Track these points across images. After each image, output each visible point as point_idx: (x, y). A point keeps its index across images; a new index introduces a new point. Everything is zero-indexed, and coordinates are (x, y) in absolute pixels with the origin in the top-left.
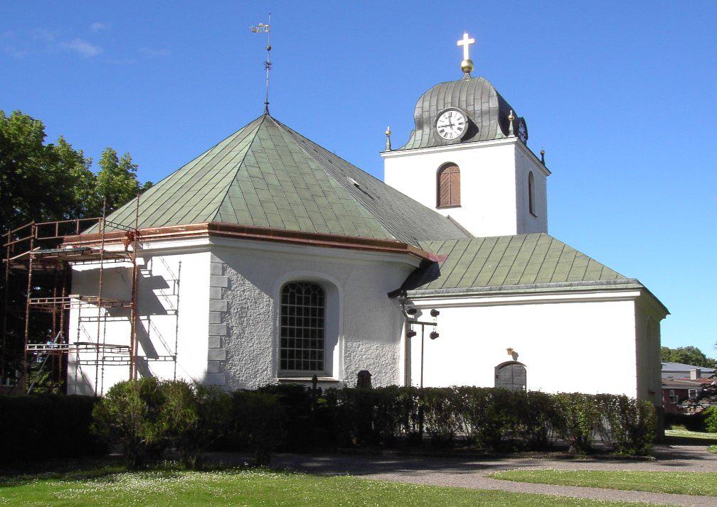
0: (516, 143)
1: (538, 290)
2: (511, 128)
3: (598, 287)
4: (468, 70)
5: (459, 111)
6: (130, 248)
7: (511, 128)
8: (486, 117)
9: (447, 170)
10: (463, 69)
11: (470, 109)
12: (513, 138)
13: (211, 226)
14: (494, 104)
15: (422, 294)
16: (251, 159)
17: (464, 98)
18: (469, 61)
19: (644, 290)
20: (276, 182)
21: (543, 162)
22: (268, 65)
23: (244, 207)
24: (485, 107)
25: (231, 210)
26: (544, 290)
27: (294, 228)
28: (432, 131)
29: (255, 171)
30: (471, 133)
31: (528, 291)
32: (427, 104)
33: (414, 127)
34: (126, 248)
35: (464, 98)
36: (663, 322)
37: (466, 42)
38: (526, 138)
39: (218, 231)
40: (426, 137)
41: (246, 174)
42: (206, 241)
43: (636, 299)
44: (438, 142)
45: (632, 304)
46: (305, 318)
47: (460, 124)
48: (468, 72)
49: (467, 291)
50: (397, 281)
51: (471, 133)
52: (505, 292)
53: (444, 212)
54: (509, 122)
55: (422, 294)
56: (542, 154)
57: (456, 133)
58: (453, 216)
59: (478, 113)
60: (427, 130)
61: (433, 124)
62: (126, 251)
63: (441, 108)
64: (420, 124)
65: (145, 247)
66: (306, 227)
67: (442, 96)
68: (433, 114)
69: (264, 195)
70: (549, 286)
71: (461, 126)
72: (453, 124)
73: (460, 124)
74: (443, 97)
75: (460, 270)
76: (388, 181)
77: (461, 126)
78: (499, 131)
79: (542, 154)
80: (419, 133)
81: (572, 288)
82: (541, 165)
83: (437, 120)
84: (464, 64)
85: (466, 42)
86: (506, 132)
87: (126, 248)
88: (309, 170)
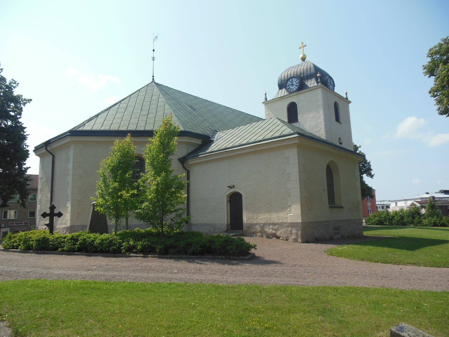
2: (319, 80)
7: (319, 80)
21: (347, 99)
22: (153, 59)
33: (277, 88)
38: (334, 86)
47: (296, 83)
56: (346, 94)
71: (297, 84)
73: (296, 83)
77: (297, 84)
79: (346, 94)
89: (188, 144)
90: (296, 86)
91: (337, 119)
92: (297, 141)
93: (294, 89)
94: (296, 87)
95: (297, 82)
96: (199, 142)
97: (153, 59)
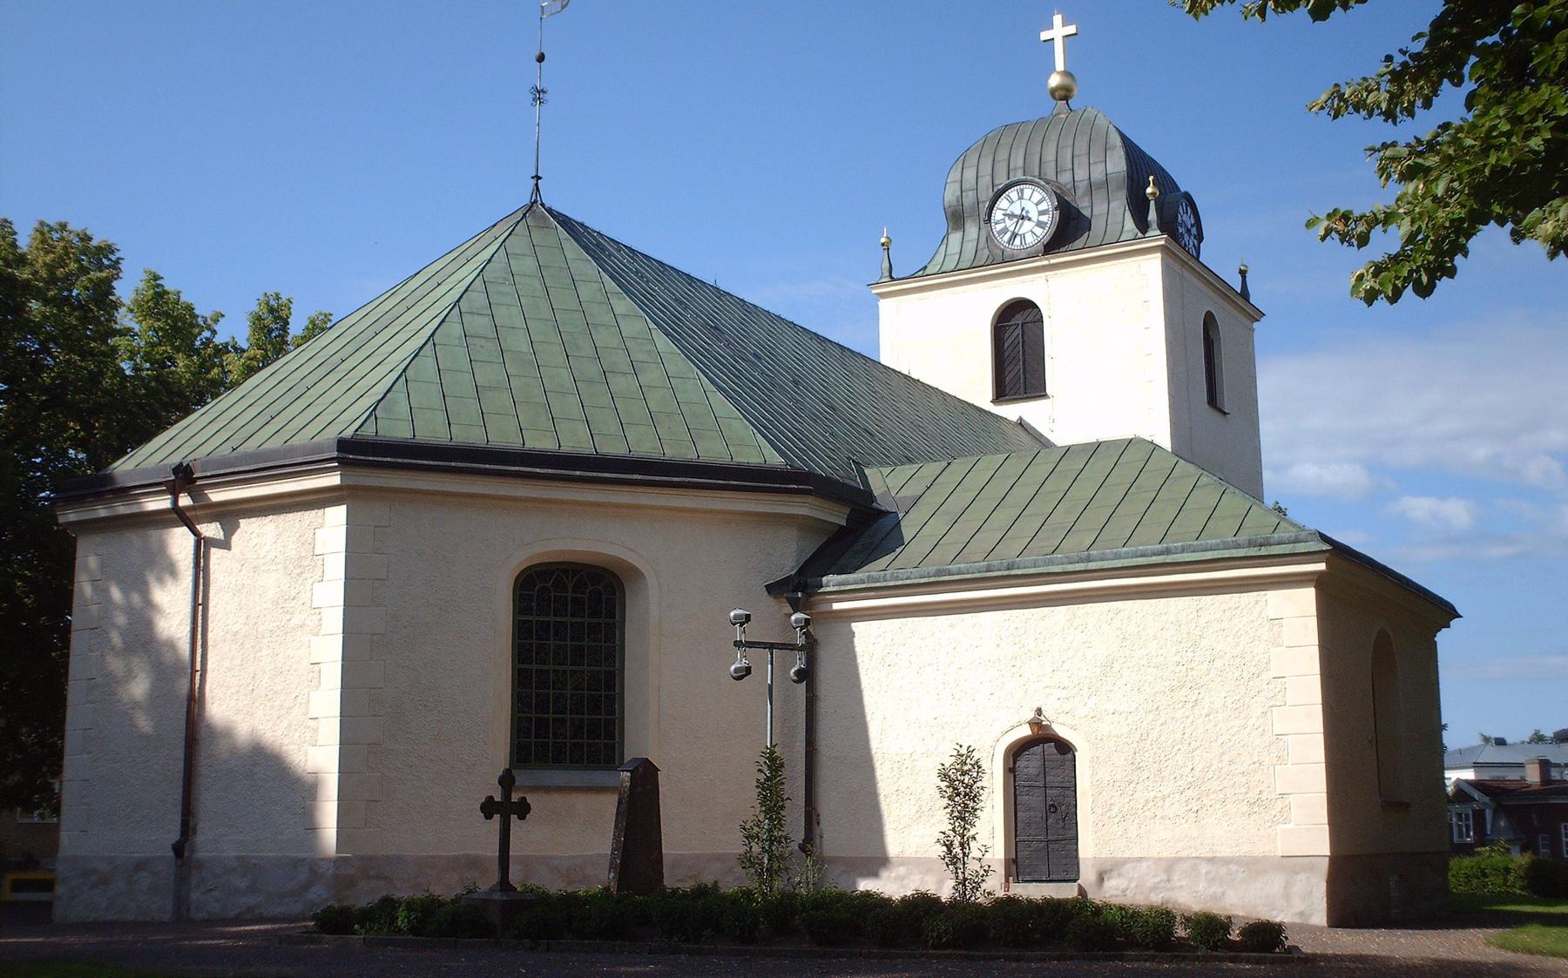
0: (1164, 249)
1: (1092, 566)
2: (1152, 216)
3: (1226, 554)
4: (1063, 93)
5: (1038, 185)
6: (185, 501)
7: (1152, 216)
8: (1099, 196)
9: (1018, 319)
10: (1053, 92)
11: (1065, 178)
12: (1156, 238)
13: (343, 445)
14: (1117, 164)
15: (840, 584)
16: (477, 299)
17: (1050, 155)
18: (1066, 73)
19: (1339, 553)
20: (525, 347)
21: (1245, 294)
22: (539, 94)
23: (436, 401)
24: (1098, 174)
25: (405, 408)
26: (1106, 564)
27: (546, 444)
28: (983, 233)
29: (480, 324)
30: (1068, 231)
31: (1070, 568)
32: (970, 175)
33: (943, 224)
34: (175, 502)
35: (1050, 155)
36: (1443, 638)
37: (1058, 31)
38: (1200, 237)
39: (356, 453)
40: (970, 248)
41: (457, 330)
42: (334, 479)
43: (1318, 581)
44: (996, 259)
45: (1308, 595)
46: (570, 661)
47: (1041, 213)
48: (1066, 98)
49: (939, 573)
50: (786, 556)
51: (1068, 231)
52: (1019, 572)
53: (1011, 411)
54: (1162, 206)
55: (840, 584)
56: (1243, 273)
57: (1034, 233)
58: (1028, 419)
59: (1082, 187)
60: (972, 230)
61: (983, 216)
62: (175, 508)
63: (1002, 181)
64: (957, 218)
65: (216, 496)
66: (575, 441)
67: (1002, 155)
68: (985, 196)
69: (489, 374)
70: (1117, 557)
71: (1044, 218)
72: (1028, 213)
73: (1041, 213)
74: (1006, 156)
75: (937, 527)
76: (886, 359)
77: (1044, 218)
78: (1130, 224)
79: (1243, 273)
80: (955, 238)
81: (1169, 559)
82: (1240, 302)
83: (991, 208)
84: (1055, 81)
85: (1058, 31)
86: (1143, 226)
87: (175, 502)
88: (608, 318)
89: (805, 525)
90: (1040, 224)
91: (1213, 399)
92: (1322, 567)
93: (1030, 239)
94: (1039, 231)
95: (1044, 206)
96: (837, 516)
97: (539, 94)
